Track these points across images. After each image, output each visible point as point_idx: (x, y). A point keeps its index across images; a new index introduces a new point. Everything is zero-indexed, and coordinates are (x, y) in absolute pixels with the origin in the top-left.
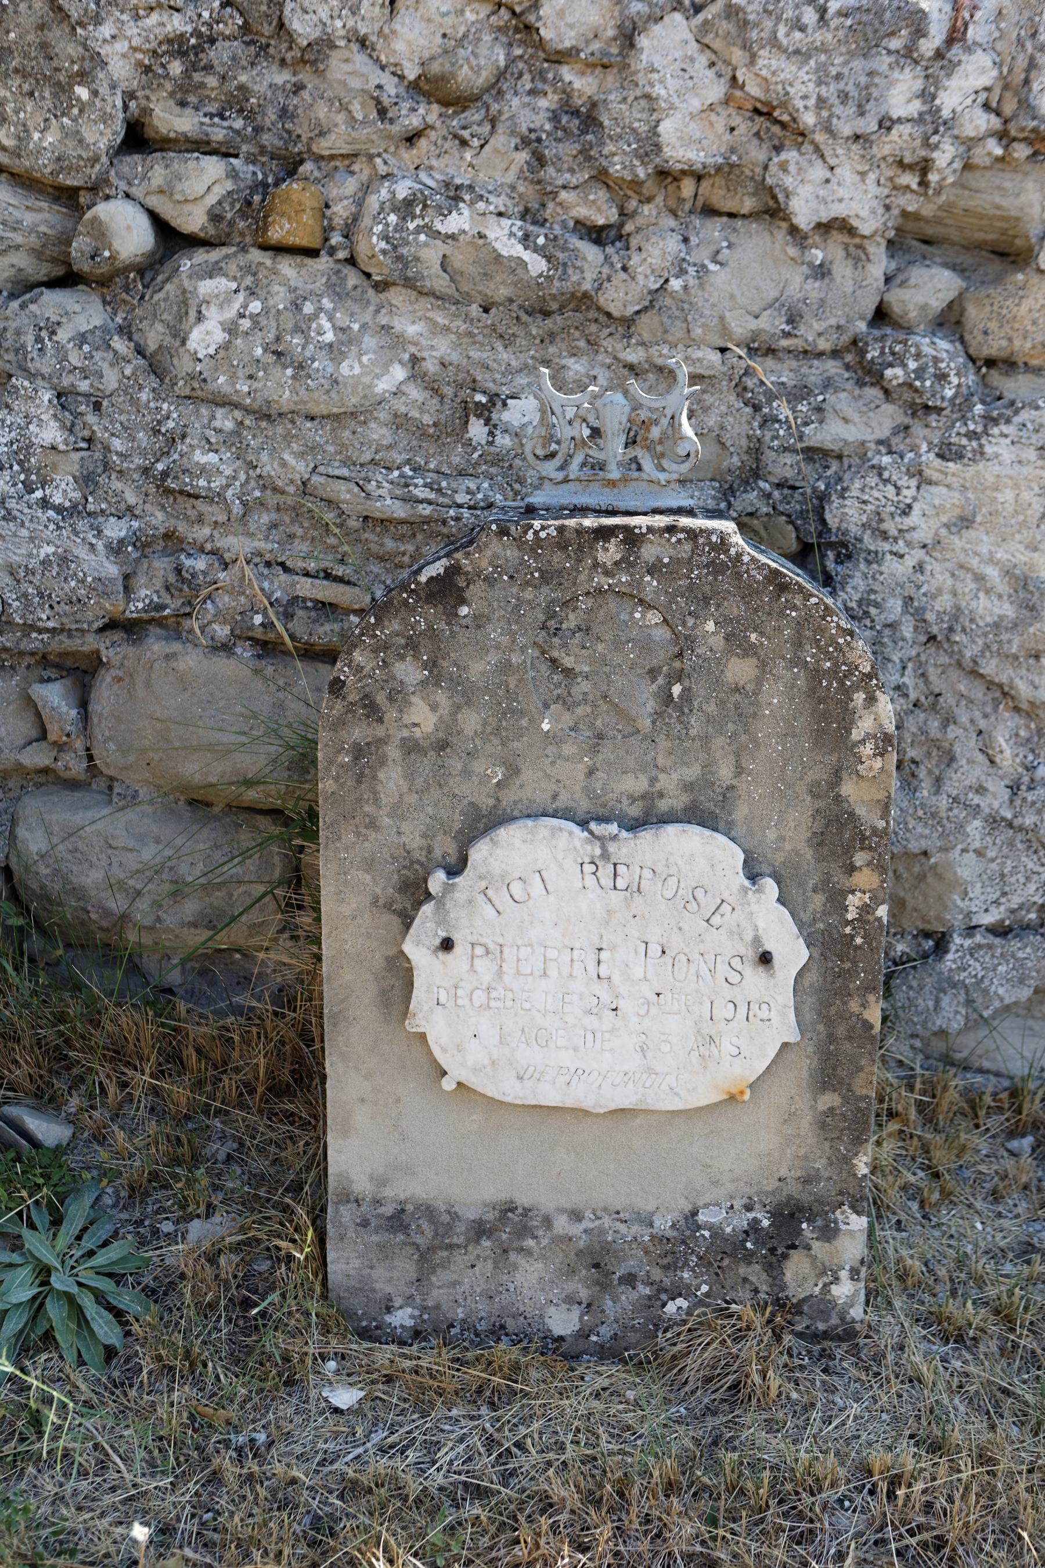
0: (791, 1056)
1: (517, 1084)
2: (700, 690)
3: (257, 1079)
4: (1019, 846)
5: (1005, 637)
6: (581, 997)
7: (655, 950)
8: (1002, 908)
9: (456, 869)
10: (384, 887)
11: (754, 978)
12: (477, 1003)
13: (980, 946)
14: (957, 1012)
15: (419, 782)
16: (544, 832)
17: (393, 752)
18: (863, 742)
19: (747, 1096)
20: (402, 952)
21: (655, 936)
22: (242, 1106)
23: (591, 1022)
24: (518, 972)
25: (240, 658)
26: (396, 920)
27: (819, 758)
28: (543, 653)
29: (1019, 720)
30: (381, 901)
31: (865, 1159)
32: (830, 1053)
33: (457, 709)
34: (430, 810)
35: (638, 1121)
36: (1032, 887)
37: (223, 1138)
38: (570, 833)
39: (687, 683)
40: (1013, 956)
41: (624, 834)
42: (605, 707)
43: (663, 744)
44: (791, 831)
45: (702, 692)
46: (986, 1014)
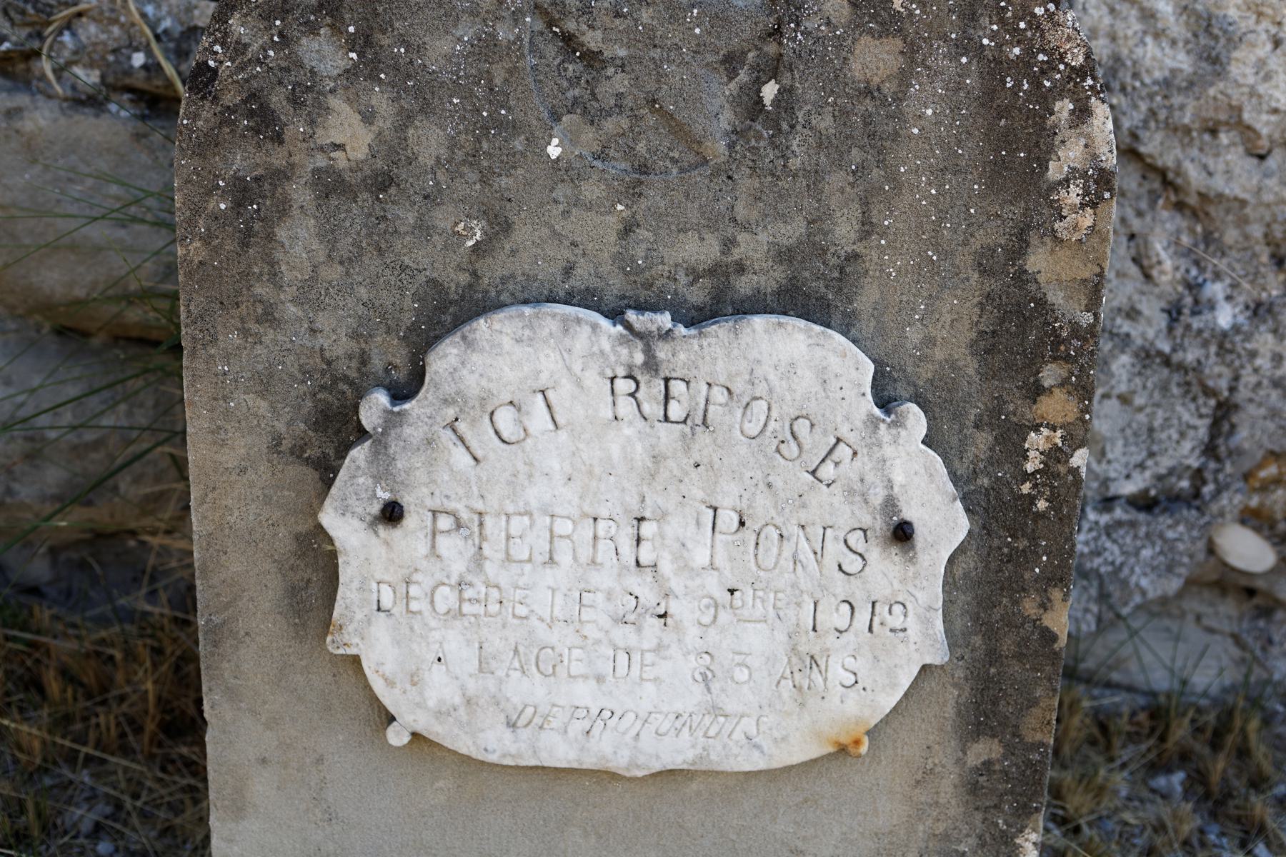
0: (931, 684)
1: (508, 734)
2: (808, 92)
3: (146, 712)
4: (1175, 390)
5: (1177, 100)
6: (609, 596)
7: (728, 519)
8: (1148, 474)
9: (406, 388)
10: (285, 417)
11: (884, 567)
12: (441, 607)
13: (1119, 524)
14: (1086, 610)
15: (345, 244)
16: (551, 326)
17: (300, 193)
18: (1065, 183)
19: (864, 749)
20: (320, 527)
21: (729, 496)
22: (126, 751)
23: (624, 635)
24: (508, 558)
25: (116, 116)
26: (311, 475)
27: (995, 208)
28: (550, 23)
29: (1181, 222)
30: (286, 445)
31: (1034, 837)
32: (989, 679)
33: (406, 119)
34: (363, 292)
35: (694, 786)
36: (1187, 445)
37: (92, 798)
38: (595, 327)
39: (786, 80)
40: (1161, 536)
41: (681, 330)
42: (651, 120)
43: (746, 183)
44: (946, 327)
45: (812, 95)
46: (1125, 611)
